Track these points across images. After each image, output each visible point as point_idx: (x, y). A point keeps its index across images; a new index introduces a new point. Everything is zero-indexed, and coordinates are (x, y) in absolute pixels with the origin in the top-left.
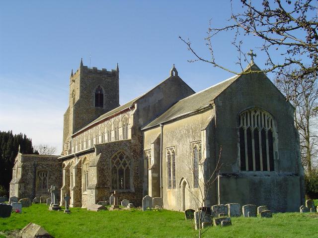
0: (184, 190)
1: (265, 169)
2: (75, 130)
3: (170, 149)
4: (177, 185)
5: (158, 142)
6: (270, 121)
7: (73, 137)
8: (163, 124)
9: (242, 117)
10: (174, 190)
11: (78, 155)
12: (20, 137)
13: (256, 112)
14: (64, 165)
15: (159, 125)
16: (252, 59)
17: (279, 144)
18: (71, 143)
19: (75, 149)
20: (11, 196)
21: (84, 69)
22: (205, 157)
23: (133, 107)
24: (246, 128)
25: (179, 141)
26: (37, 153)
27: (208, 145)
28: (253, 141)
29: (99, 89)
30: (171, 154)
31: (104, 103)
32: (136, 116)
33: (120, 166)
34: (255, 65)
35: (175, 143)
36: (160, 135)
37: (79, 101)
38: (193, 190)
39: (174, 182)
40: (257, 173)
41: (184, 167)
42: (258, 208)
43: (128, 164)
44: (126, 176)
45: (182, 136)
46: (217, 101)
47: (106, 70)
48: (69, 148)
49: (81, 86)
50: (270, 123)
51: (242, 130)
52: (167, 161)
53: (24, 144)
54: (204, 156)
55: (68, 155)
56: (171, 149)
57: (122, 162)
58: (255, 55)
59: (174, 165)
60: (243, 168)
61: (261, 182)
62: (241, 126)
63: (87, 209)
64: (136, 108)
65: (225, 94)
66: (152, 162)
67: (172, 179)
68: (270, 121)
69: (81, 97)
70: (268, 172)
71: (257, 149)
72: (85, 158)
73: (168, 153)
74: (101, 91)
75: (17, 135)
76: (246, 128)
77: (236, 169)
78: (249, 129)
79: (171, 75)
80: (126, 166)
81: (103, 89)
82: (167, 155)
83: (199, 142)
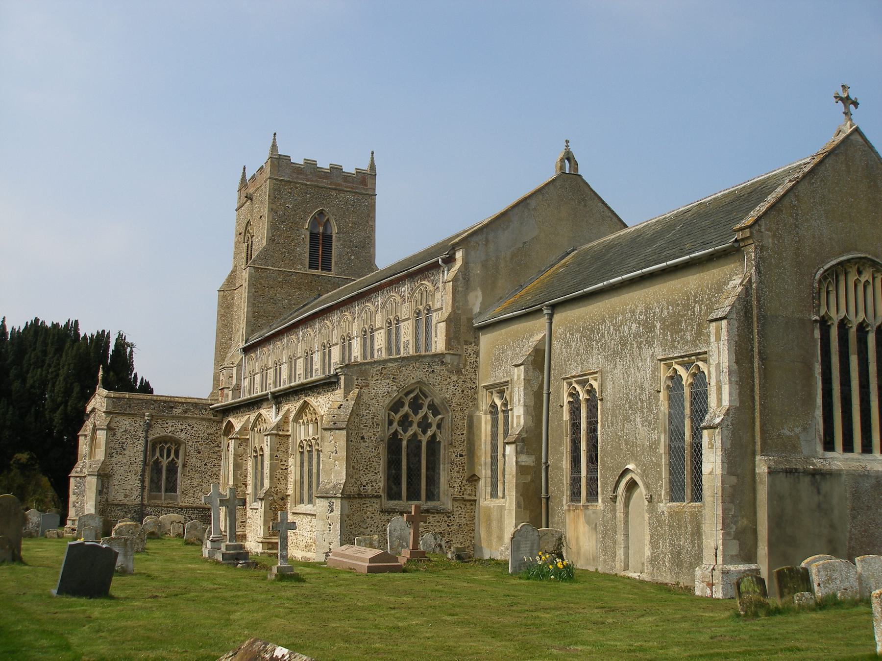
2: (253, 326)
3: (577, 382)
5: (538, 360)
7: (246, 350)
8: (554, 307)
11: (279, 398)
13: (860, 273)
14: (230, 426)
16: (847, 113)
19: (252, 383)
20: (72, 513)
21: (278, 161)
22: (726, 403)
24: (835, 317)
25: (615, 355)
26: (146, 388)
27: (735, 367)
28: (854, 360)
30: (583, 396)
34: (857, 130)
35: (595, 362)
39: (592, 481)
43: (434, 428)
47: (58, 324)
48: (234, 382)
49: (271, 210)
51: (824, 324)
53: (103, 362)
54: (721, 399)
55: (259, 394)
56: (583, 383)
58: (856, 104)
60: (829, 446)
62: (823, 312)
63: (681, 584)
64: (459, 263)
69: (271, 240)
75: (89, 335)
76: (835, 317)
80: (429, 433)
81: (333, 223)
82: (566, 399)
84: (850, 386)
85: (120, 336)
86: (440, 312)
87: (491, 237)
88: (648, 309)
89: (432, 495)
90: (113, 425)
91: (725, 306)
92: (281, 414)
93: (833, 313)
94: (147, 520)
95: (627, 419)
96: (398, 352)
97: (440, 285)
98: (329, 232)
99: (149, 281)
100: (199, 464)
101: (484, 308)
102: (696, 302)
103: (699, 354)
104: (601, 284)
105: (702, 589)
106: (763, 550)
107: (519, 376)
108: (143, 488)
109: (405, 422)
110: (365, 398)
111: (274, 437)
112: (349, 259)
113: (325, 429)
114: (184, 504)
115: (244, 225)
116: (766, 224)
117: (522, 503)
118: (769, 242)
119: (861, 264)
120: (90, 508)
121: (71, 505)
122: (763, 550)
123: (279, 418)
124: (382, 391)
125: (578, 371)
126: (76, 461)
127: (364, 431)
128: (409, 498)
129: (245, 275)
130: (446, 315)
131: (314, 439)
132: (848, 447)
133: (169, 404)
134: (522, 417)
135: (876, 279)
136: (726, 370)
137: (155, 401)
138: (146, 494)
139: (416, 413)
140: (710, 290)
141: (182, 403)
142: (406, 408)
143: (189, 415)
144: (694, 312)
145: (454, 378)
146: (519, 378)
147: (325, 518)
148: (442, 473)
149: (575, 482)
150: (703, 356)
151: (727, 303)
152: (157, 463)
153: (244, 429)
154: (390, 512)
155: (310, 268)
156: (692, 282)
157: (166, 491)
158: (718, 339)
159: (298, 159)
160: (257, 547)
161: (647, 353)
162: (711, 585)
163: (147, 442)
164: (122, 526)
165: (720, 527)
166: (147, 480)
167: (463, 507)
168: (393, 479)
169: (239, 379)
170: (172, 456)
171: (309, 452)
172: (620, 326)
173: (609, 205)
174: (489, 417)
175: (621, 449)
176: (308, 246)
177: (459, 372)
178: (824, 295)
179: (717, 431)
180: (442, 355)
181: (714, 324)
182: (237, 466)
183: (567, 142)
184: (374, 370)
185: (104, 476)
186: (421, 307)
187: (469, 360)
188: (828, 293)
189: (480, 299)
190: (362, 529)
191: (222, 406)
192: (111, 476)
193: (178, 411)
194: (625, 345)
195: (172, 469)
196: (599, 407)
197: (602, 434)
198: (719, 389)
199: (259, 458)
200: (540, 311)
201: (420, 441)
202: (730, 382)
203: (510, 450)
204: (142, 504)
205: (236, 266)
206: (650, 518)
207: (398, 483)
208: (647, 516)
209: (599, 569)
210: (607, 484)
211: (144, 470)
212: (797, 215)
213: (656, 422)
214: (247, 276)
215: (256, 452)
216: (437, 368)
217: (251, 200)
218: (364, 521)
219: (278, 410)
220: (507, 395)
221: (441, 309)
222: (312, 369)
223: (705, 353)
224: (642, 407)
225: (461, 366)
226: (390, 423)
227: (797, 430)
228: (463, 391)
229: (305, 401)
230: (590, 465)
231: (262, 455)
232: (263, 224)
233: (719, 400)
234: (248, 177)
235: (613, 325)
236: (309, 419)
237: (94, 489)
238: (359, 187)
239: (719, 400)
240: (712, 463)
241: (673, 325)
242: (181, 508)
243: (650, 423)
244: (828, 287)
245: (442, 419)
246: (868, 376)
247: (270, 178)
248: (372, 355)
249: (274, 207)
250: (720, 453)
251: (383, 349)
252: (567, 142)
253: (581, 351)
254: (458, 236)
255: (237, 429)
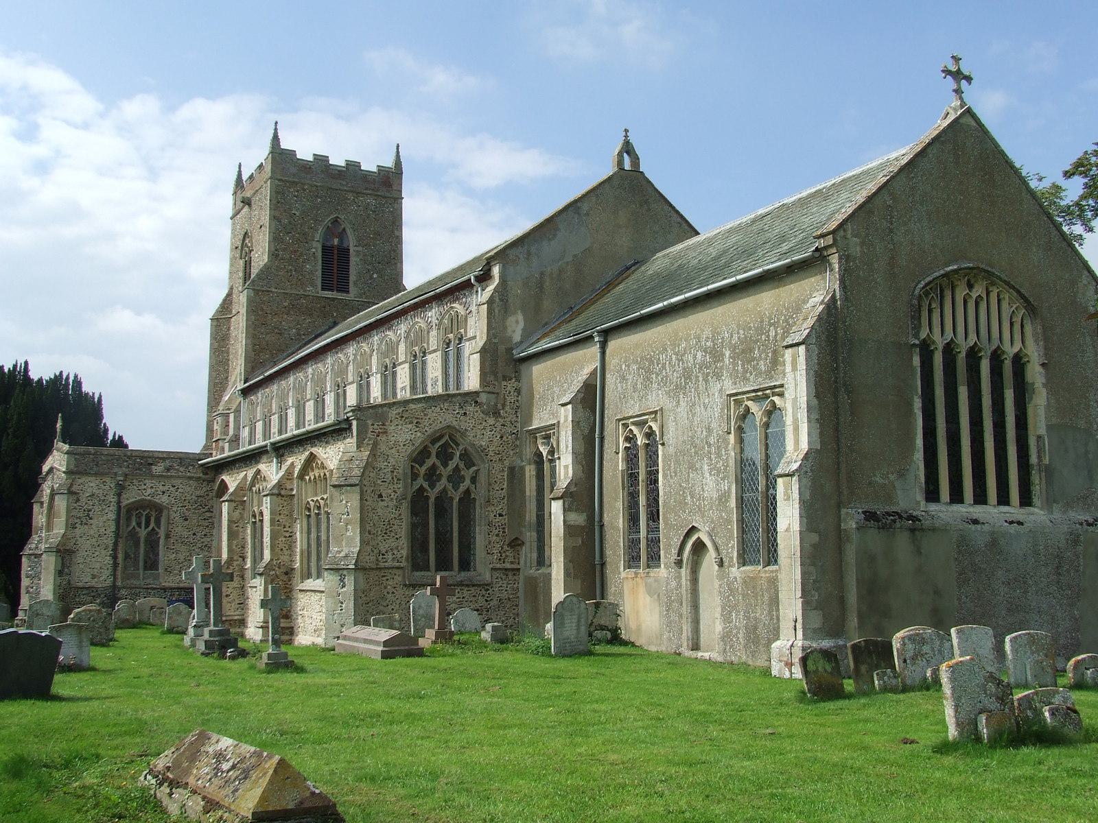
0: (694, 580)
1: (1003, 499)
2: (253, 365)
3: (633, 423)
4: (667, 554)
5: (590, 399)
6: (1017, 320)
7: (245, 392)
8: (607, 334)
9: (925, 303)
10: (654, 572)
11: (281, 449)
12: (58, 382)
14: (224, 487)
15: (591, 337)
17: (1048, 407)
18: (237, 411)
20: (25, 602)
21: (281, 157)
22: (804, 446)
23: (484, 277)
24: (939, 342)
25: (678, 390)
26: (119, 443)
27: (815, 402)
28: (963, 392)
29: (335, 228)
30: (641, 440)
31: (352, 278)
32: (498, 309)
33: (439, 487)
34: (969, 111)
35: (656, 399)
36: (594, 373)
37: (266, 270)
38: (735, 572)
39: (654, 543)
40: (978, 511)
41: (700, 491)
42: (1008, 639)
43: (467, 482)
44: (458, 529)
45: (687, 375)
46: (845, 237)
47: (357, 165)
48: (231, 432)
49: (273, 218)
50: (1017, 327)
51: (926, 349)
52: (621, 466)
53: (63, 410)
54: (798, 438)
55: (227, 454)
56: (641, 424)
57: (446, 472)
59: (653, 480)
60: (932, 494)
61: (993, 542)
62: (923, 335)
64: (496, 281)
65: (871, 212)
66: (565, 468)
67: (643, 533)
68: (1017, 320)
69: (274, 255)
70: (1014, 510)
71: (976, 423)
72: (312, 457)
73: (628, 439)
74: (342, 235)
76: (939, 342)
77: (910, 497)
78: (949, 349)
79: (616, 169)
80: (463, 487)
82: (622, 445)
83: (768, 394)
84: (958, 423)
85: (76, 376)
86: (473, 341)
87: (533, 249)
88: (716, 333)
89: (465, 565)
90: (74, 489)
91: (802, 329)
92: (284, 467)
93: (936, 336)
94: (120, 605)
95: (692, 467)
96: (424, 391)
97: (473, 308)
98: (345, 245)
99: (132, 306)
100: (185, 534)
101: (527, 334)
102: (771, 325)
103: (775, 387)
104: (660, 305)
105: (780, 670)
106: (853, 621)
107: (566, 417)
108: (115, 565)
109: (432, 476)
110: (383, 447)
111: (275, 497)
112: (371, 277)
113: (334, 486)
114: (167, 584)
115: (241, 237)
116: (853, 230)
117: (572, 570)
118: (856, 250)
119: (971, 276)
120: (47, 591)
121: (23, 591)
122: (853, 621)
123: (281, 473)
124: (403, 438)
125: (636, 410)
126: (29, 535)
127: (381, 488)
128: (438, 569)
129: (243, 299)
130: (481, 344)
131: (322, 499)
132: (957, 497)
133: (146, 461)
134: (571, 467)
135: (991, 294)
136: (804, 406)
137: (130, 457)
138: (119, 573)
139: (445, 465)
140: (787, 309)
141: (164, 459)
142: (433, 460)
143: (173, 473)
144: (768, 336)
145: (491, 421)
146: (566, 420)
147: (335, 594)
148: (477, 536)
149: (633, 544)
150: (779, 391)
151: (805, 326)
152: (133, 535)
153: (240, 488)
154: (415, 586)
155: (323, 289)
156: (766, 300)
157: (145, 568)
158: (794, 369)
159: (305, 153)
160: (256, 634)
161: (715, 387)
162: (790, 665)
163: (119, 508)
164: (80, 612)
165: (799, 594)
166: (120, 556)
167: (504, 577)
168: (418, 545)
169: (237, 428)
170: (152, 525)
171: (316, 517)
172: (683, 355)
173: (677, 208)
174: (533, 467)
175: (686, 504)
176: (320, 262)
177: (496, 414)
178: (925, 314)
179: (794, 479)
180: (476, 393)
181: (790, 350)
182: (232, 535)
183: (626, 131)
184: (393, 413)
185: (65, 553)
186: (451, 336)
187: (508, 399)
188: (930, 311)
189: (522, 325)
190: (381, 608)
191: (214, 461)
192: (74, 552)
193: (158, 469)
194: (689, 377)
195: (152, 543)
196: (660, 453)
197: (664, 485)
198: (796, 429)
199: (258, 524)
200: (591, 337)
201: (427, 498)
202: (809, 421)
203: (556, 508)
204: (114, 586)
205: (231, 288)
206: (720, 585)
207: (424, 549)
208: (717, 583)
209: (64, 470)
210: (670, 545)
211: (116, 544)
212: (892, 217)
213: (725, 469)
214: (245, 300)
215: (255, 517)
216: (470, 409)
217: (249, 204)
218: (383, 598)
219: (280, 463)
220: (553, 441)
221: (474, 337)
222: (324, 414)
223: (782, 386)
224: (710, 452)
225: (499, 406)
226: (415, 476)
227: (892, 477)
228: (501, 437)
229: (311, 453)
230: (651, 523)
231: (262, 521)
232: (264, 235)
233: (797, 442)
234: (245, 177)
235: (676, 354)
236: (317, 475)
237: (52, 568)
238: (384, 188)
239: (797, 442)
240: (789, 517)
241: (744, 352)
242: (165, 589)
243: (719, 472)
244: (930, 304)
245: (477, 472)
246: (981, 411)
247: (271, 178)
248: (395, 394)
249: (277, 214)
250: (797, 506)
251: (408, 387)
252: (626, 131)
253: (639, 386)
254: (492, 250)
255: (231, 490)
